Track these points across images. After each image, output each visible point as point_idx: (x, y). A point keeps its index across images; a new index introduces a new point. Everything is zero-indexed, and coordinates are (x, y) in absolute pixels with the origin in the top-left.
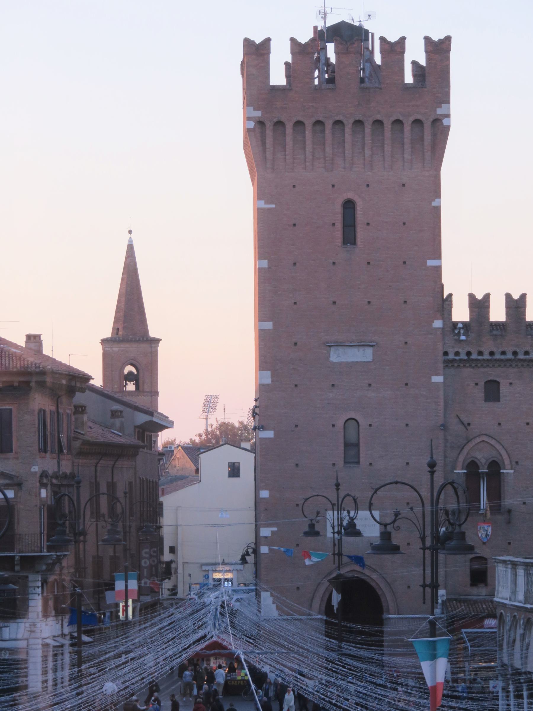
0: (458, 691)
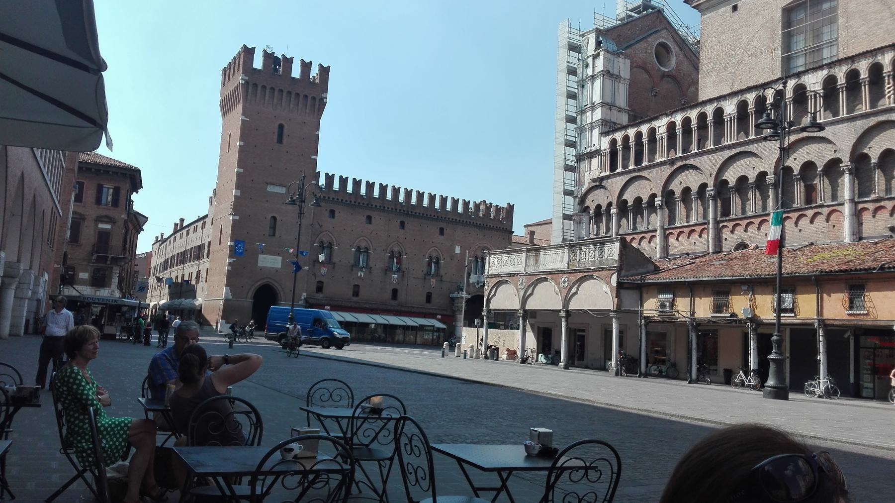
0: (619, 226)
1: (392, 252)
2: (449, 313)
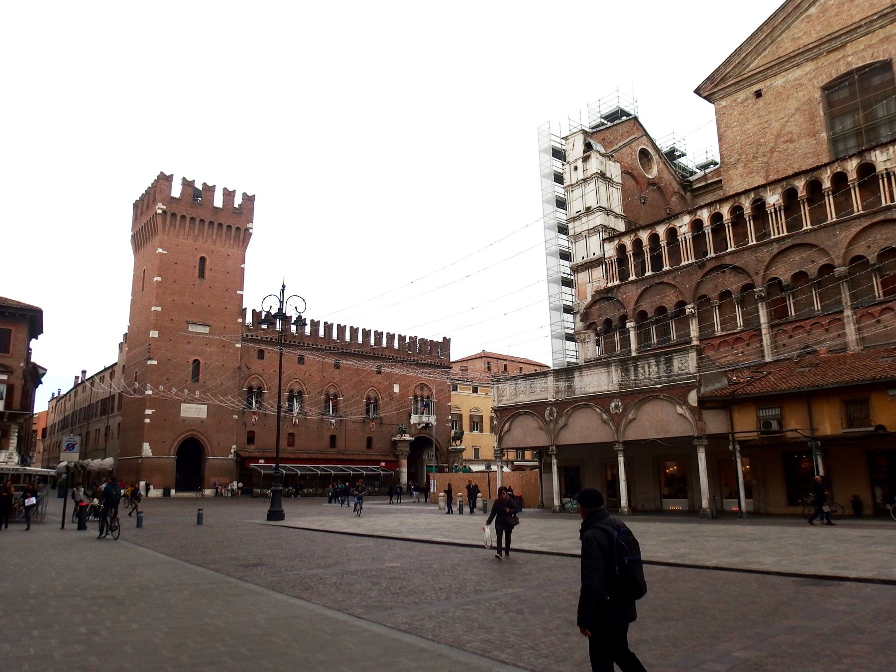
1: (327, 395)
2: (392, 458)
